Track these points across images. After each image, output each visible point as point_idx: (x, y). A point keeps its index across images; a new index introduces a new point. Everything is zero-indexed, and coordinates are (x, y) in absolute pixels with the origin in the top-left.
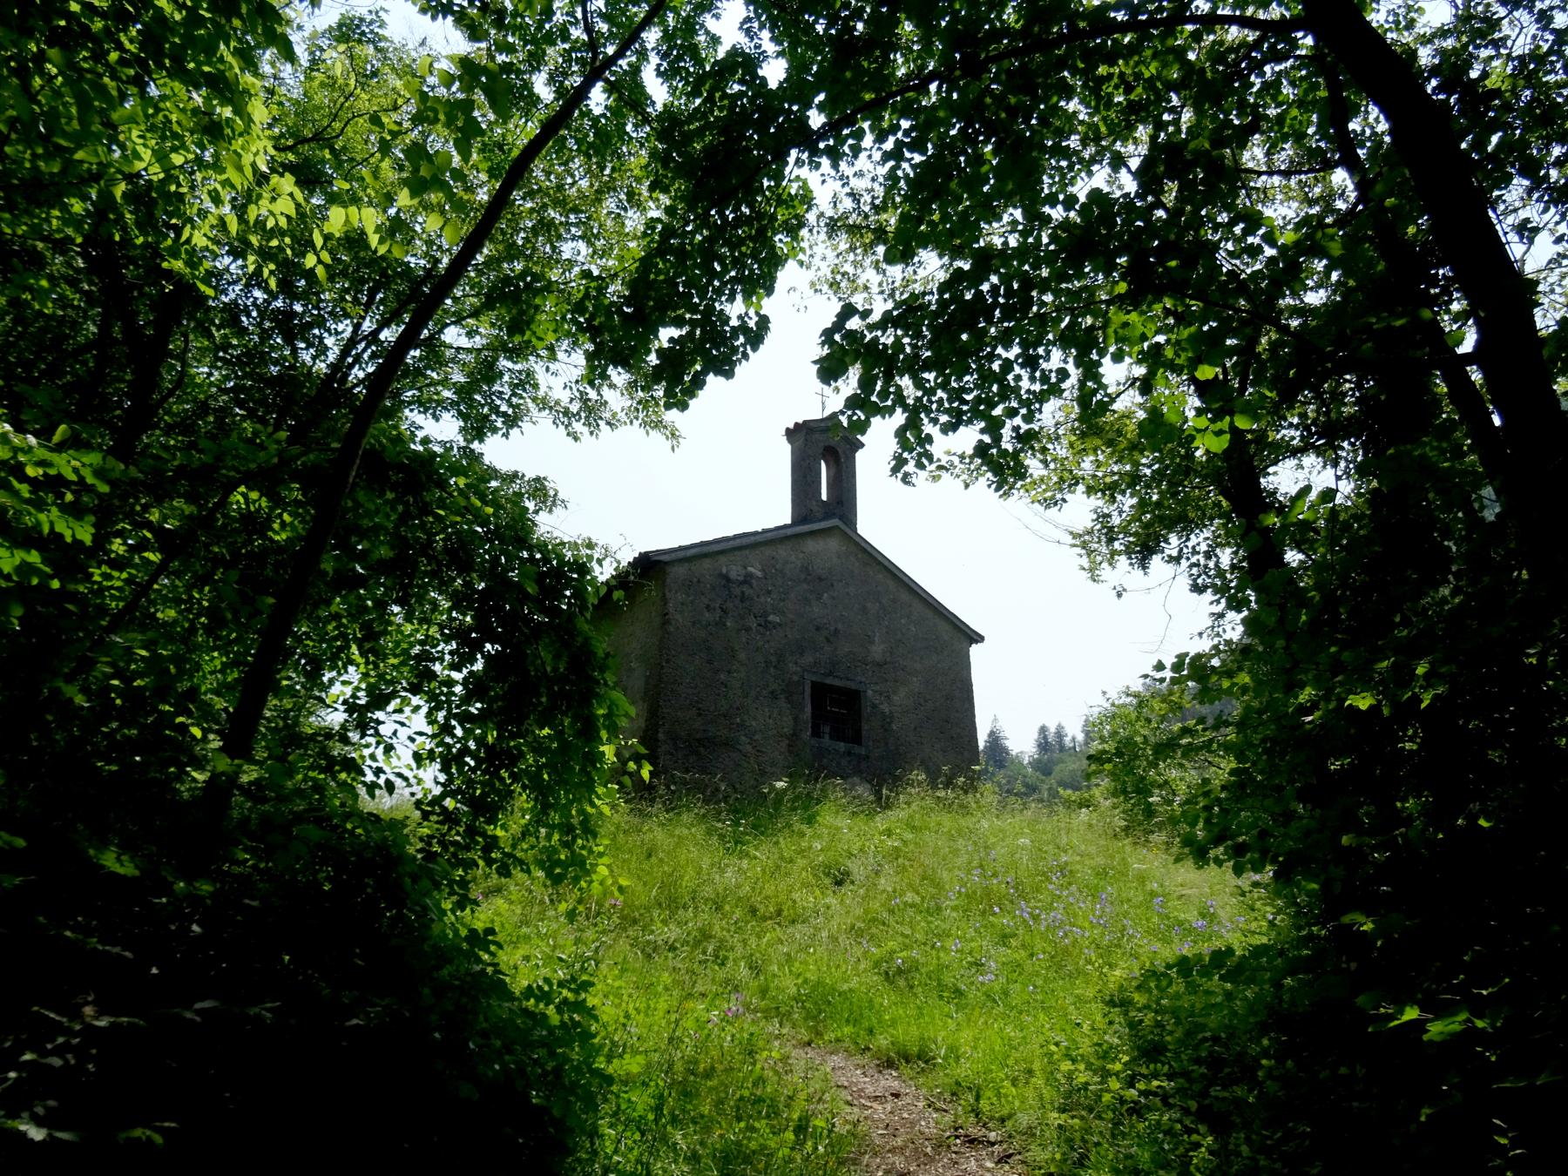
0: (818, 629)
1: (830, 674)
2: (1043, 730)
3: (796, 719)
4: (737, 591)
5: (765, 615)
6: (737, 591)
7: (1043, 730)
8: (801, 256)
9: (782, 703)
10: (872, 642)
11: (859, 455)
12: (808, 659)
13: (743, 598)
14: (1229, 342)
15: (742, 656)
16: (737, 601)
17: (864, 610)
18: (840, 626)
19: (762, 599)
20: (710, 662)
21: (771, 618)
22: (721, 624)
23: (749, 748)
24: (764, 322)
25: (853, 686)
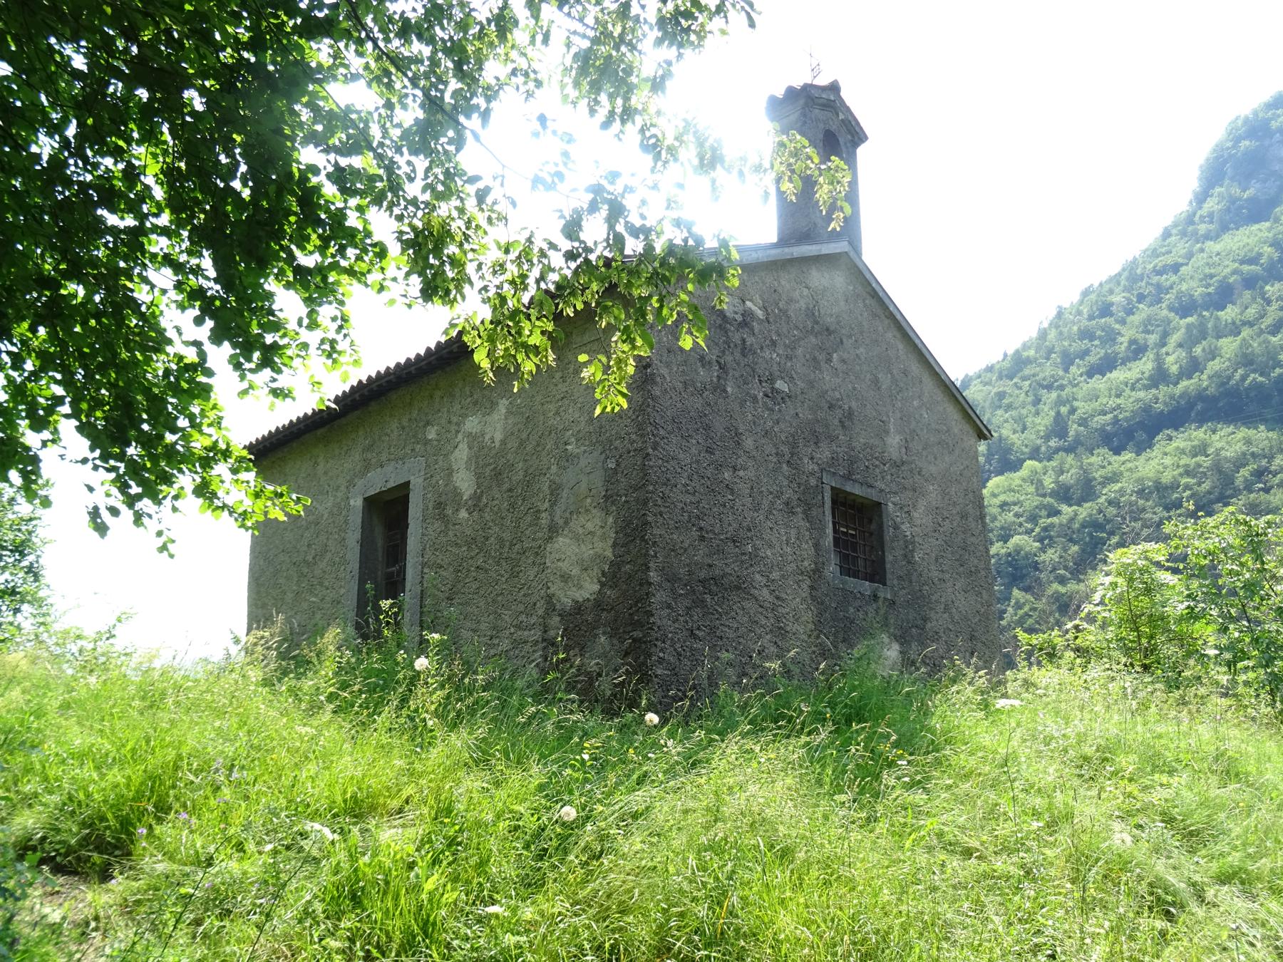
0: (831, 407)
1: (848, 477)
2: (663, 92)
3: (817, 546)
4: (736, 338)
5: (771, 380)
6: (736, 338)
7: (663, 92)
8: (194, 820)
9: (799, 520)
10: (887, 432)
11: (844, 94)
12: (824, 453)
13: (745, 350)
14: (13, 48)
15: (749, 443)
16: (738, 355)
17: (876, 381)
18: (854, 404)
19: (767, 354)
20: (710, 451)
21: (779, 384)
22: (719, 389)
23: (765, 592)
24: (243, 526)
25: (873, 495)
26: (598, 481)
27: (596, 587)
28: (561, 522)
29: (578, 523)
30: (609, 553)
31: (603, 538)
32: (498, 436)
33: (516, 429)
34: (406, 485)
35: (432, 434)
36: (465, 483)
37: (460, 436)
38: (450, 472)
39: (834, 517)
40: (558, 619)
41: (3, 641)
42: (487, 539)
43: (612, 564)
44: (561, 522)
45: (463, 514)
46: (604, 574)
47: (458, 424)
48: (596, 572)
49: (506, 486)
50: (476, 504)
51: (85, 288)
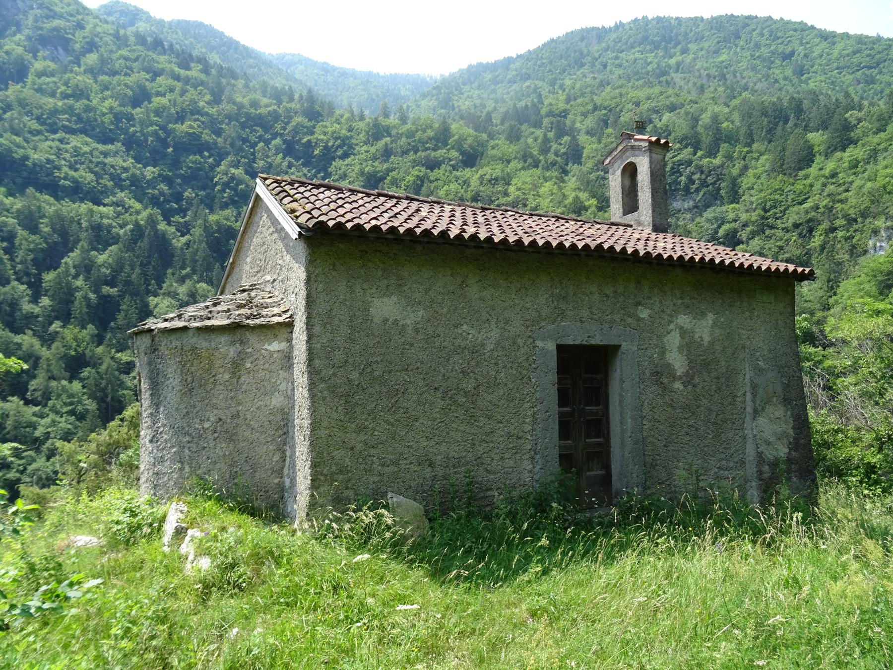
26: (779, 389)
27: (787, 450)
28: (760, 408)
29: (769, 409)
30: (791, 432)
31: (786, 422)
32: (707, 338)
33: (721, 338)
34: (618, 347)
35: (644, 314)
36: (678, 362)
37: (672, 326)
38: (663, 351)
39: (313, 397)
40: (767, 467)
41: (15, 385)
42: (698, 407)
43: (795, 439)
44: (760, 408)
45: (678, 385)
46: (790, 443)
47: (672, 316)
48: (785, 441)
49: (713, 375)
50: (688, 380)
51: (167, 269)
